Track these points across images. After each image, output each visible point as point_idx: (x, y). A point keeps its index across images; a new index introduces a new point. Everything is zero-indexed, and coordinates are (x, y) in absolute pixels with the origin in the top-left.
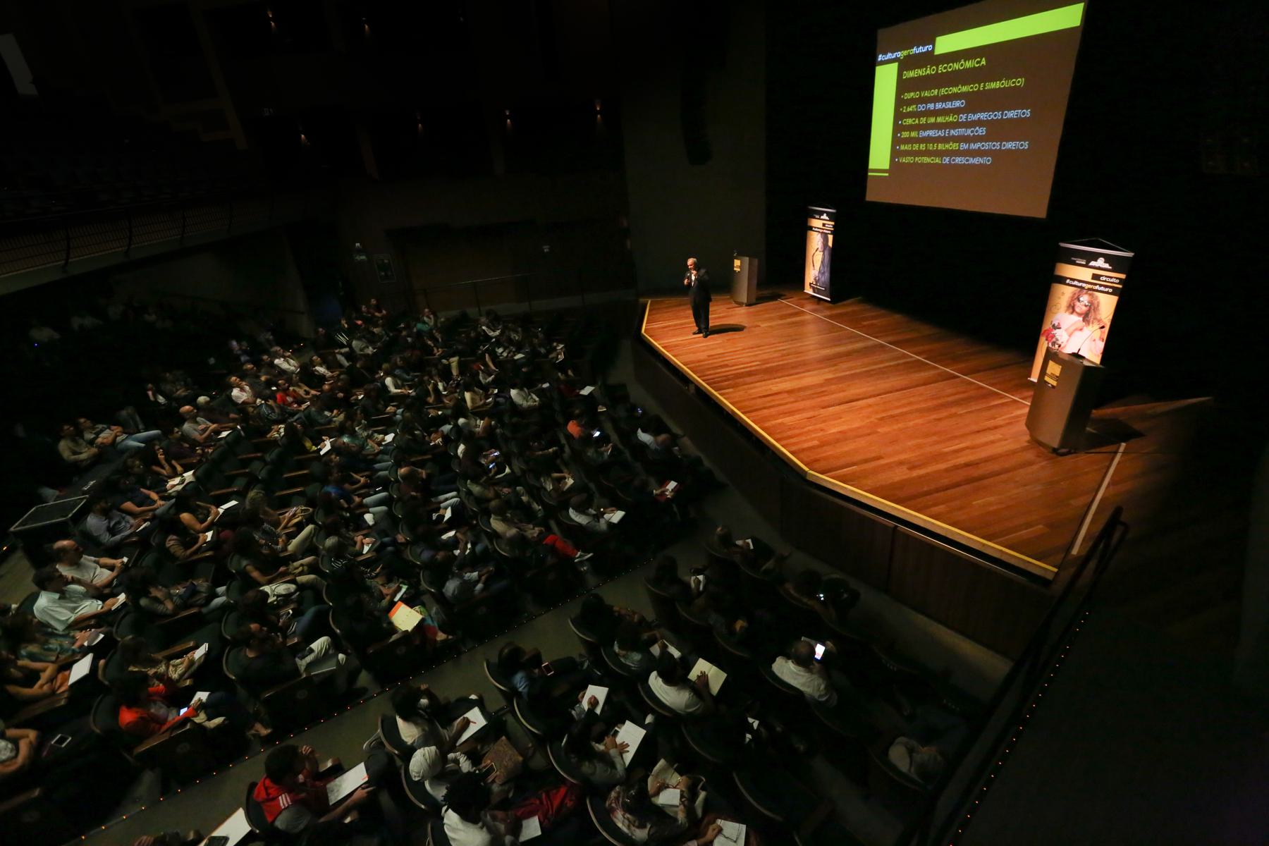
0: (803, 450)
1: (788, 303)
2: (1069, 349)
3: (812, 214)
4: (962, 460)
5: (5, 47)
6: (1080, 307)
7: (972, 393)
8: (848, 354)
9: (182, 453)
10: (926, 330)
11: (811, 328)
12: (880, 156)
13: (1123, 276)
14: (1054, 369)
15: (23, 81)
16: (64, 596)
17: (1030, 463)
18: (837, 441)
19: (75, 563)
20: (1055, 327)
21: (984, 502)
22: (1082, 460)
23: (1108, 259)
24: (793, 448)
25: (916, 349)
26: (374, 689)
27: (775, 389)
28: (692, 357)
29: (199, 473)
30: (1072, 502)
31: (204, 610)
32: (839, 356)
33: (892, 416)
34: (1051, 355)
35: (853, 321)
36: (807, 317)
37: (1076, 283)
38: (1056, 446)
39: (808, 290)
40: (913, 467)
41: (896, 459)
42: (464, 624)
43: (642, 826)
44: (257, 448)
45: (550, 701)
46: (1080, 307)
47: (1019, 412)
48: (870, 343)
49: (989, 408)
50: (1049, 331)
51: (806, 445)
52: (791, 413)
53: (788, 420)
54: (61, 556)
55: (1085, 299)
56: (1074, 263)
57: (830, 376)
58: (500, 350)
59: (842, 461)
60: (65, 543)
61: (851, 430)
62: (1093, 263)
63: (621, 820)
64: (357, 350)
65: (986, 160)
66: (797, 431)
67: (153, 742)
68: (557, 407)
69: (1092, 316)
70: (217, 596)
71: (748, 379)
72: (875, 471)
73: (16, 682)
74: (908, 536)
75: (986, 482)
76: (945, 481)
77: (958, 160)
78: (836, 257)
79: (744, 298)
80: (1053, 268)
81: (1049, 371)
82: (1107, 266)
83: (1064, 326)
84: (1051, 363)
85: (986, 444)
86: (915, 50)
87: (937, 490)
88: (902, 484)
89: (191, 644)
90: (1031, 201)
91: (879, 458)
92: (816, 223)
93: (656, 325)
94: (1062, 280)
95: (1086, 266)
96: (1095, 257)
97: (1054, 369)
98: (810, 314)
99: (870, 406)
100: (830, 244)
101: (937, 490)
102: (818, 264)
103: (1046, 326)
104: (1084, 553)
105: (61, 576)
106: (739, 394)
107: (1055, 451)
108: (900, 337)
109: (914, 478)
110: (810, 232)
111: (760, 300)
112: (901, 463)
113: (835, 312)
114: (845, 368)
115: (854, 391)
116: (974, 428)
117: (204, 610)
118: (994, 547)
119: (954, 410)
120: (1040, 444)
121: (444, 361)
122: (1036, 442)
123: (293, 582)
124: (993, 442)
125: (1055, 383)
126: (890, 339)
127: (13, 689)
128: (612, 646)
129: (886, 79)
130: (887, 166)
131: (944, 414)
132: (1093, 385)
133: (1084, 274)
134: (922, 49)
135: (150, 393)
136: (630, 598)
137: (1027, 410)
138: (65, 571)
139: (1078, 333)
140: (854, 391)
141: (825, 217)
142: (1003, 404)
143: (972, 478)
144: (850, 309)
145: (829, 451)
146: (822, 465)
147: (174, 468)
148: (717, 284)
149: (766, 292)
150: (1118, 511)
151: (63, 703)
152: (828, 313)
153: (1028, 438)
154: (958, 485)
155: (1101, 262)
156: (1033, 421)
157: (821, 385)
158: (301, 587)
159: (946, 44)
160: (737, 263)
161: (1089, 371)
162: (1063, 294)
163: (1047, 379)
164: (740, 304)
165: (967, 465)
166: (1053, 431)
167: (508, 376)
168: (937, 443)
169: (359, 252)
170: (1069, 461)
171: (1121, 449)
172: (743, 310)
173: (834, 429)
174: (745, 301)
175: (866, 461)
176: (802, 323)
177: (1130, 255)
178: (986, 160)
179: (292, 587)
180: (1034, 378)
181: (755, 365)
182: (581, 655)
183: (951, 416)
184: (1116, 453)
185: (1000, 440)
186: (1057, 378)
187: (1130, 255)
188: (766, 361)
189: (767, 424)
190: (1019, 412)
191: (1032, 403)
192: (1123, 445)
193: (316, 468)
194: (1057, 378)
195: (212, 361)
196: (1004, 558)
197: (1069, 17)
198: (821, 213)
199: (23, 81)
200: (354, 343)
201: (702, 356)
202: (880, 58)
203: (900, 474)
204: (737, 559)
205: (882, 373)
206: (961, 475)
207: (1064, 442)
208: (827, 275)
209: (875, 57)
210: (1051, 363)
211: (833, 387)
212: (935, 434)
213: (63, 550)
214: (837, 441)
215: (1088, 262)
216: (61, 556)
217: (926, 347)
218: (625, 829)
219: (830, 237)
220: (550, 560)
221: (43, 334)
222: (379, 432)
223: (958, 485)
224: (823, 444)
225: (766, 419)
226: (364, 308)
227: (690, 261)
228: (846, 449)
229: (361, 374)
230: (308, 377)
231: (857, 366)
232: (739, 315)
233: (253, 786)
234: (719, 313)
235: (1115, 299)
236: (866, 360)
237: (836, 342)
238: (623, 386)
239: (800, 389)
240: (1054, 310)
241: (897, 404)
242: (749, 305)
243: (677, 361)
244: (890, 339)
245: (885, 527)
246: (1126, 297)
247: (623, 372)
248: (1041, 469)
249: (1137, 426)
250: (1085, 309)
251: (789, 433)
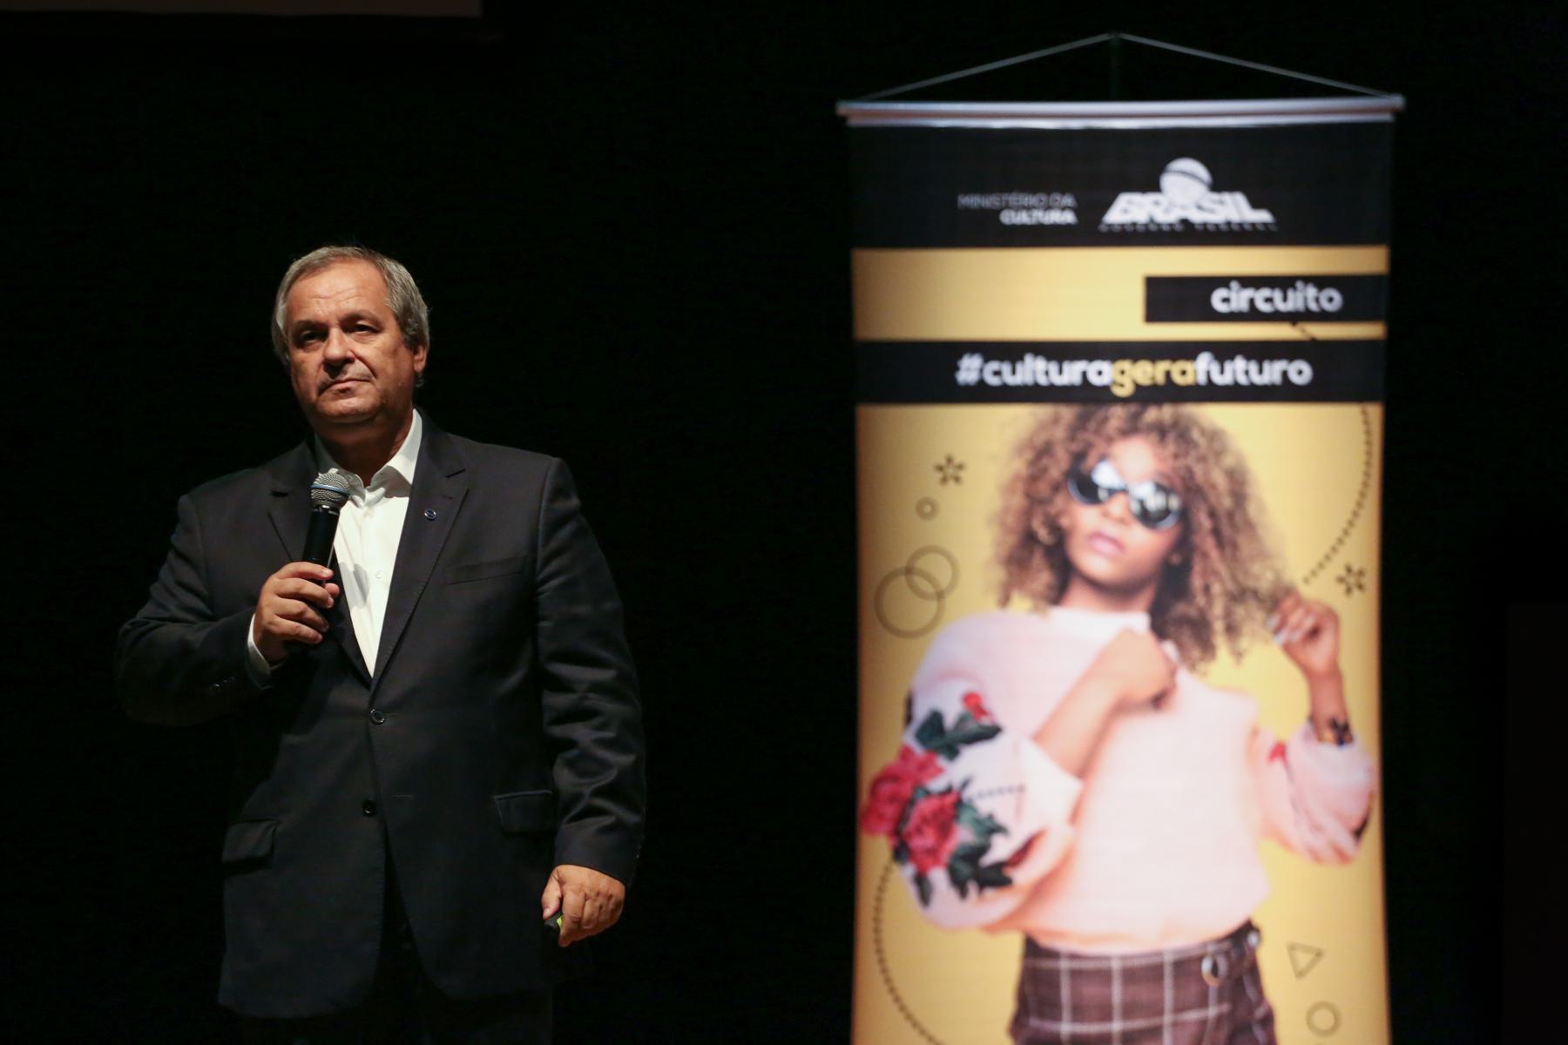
6: (1111, 539)
13: (1367, 260)
20: (943, 738)
23: (1228, 160)
37: (1033, 370)
46: (1111, 539)
50: (907, 775)
55: (1131, 467)
62: (1128, 209)
65: (1387, 117)
69: (1211, 586)
80: (837, 296)
82: (1235, 209)
94: (929, 373)
95: (1089, 232)
96: (1142, 161)
103: (885, 744)
133: (1079, 294)
139: (1140, 739)
155: (1185, 192)
162: (956, 473)
177: (863, 112)
187: (863, 112)
250: (1145, 544)
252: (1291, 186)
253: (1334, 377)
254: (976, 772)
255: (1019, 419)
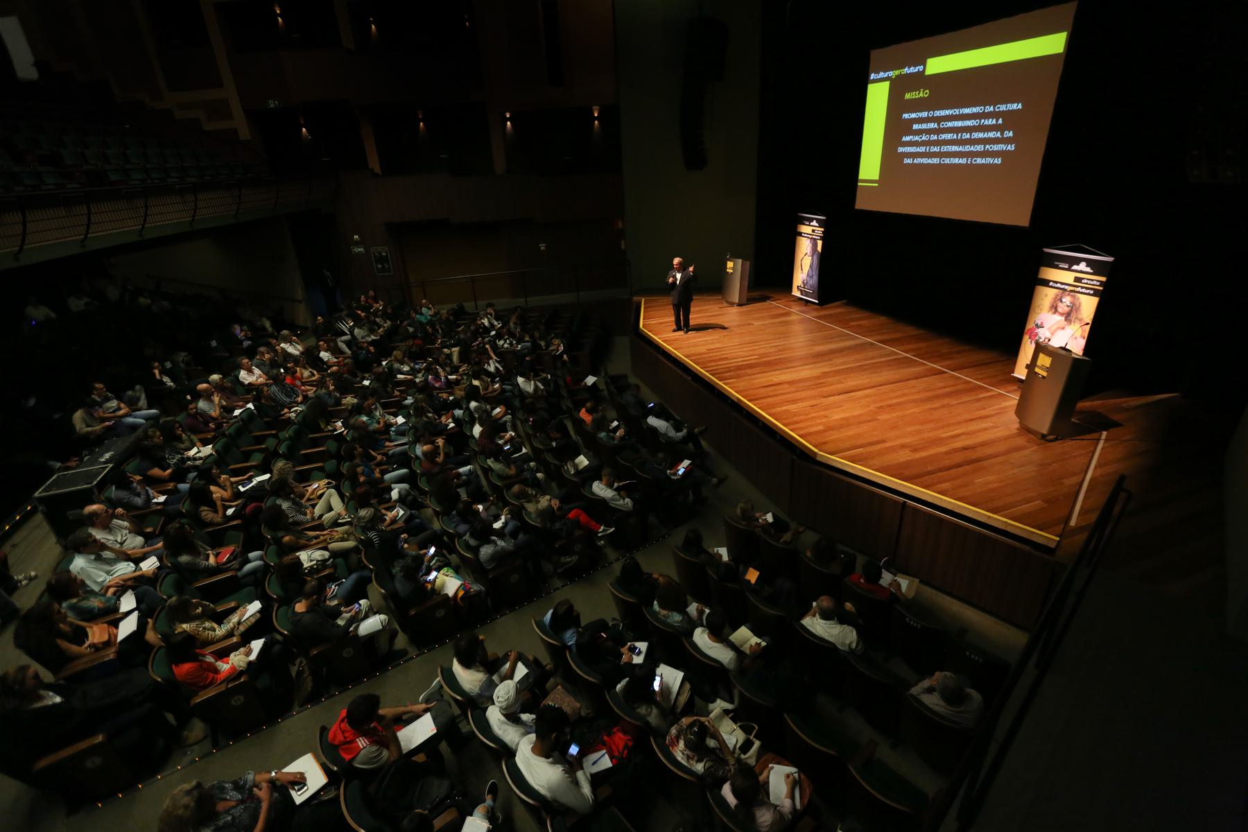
0: (811, 434)
1: (777, 305)
2: (1056, 342)
3: (802, 221)
4: (959, 444)
5: (10, 30)
6: (1063, 308)
7: (960, 387)
8: (840, 351)
9: (201, 428)
10: (911, 331)
11: (798, 328)
12: (870, 166)
13: (1104, 279)
14: (1044, 360)
15: (24, 64)
16: (99, 558)
17: (1024, 448)
18: (841, 427)
19: (107, 527)
20: (1038, 326)
21: (985, 481)
22: (1069, 446)
23: (1090, 263)
24: (801, 432)
25: (907, 347)
26: (413, 652)
27: (776, 380)
28: (693, 350)
29: (219, 445)
30: (1065, 481)
31: (239, 574)
32: (832, 352)
33: (890, 406)
34: (1040, 348)
35: (844, 323)
36: (793, 318)
38: (1045, 431)
39: (796, 293)
40: (915, 450)
41: (898, 442)
42: (502, 590)
43: (699, 761)
44: (269, 426)
45: (600, 649)
46: (1063, 308)
47: (1007, 404)
48: (857, 342)
49: (979, 400)
50: (1031, 331)
51: (813, 429)
52: (795, 401)
53: (792, 407)
54: (93, 520)
55: (1067, 300)
56: (1057, 267)
57: (826, 369)
58: (502, 342)
59: (848, 444)
60: (95, 507)
61: (853, 417)
62: (1075, 267)
63: (680, 752)
64: (359, 337)
65: (998, 161)
66: (802, 417)
67: (211, 693)
68: (564, 392)
69: (1073, 316)
70: (249, 561)
71: (749, 371)
72: (881, 453)
73: (63, 636)
74: (916, 510)
75: (984, 463)
76: (947, 462)
77: (979, 161)
78: (825, 262)
79: (736, 298)
80: (1037, 271)
81: (1039, 363)
82: (1088, 270)
83: (1047, 325)
84: (1041, 355)
85: (979, 431)
86: (906, 70)
87: (940, 470)
88: (908, 464)
89: (233, 604)
90: (1014, 210)
91: (884, 441)
92: (805, 229)
93: (652, 322)
94: (1046, 283)
95: (1069, 269)
96: (1078, 261)
97: (1044, 360)
98: (796, 312)
99: (867, 396)
100: (819, 249)
101: (940, 470)
102: (806, 268)
104: (1093, 517)
105: (95, 541)
106: (742, 384)
107: (1043, 436)
108: (886, 337)
109: (917, 460)
110: (799, 238)
111: (751, 301)
112: (903, 446)
113: (822, 313)
114: (839, 363)
115: (851, 382)
116: (967, 416)
117: (239, 574)
118: (998, 520)
119: (946, 401)
120: (1029, 431)
121: (446, 350)
122: (1025, 430)
123: (325, 549)
124: (985, 429)
125: (1045, 374)
126: (879, 338)
127: (64, 644)
128: (652, 605)
129: (877, 97)
130: (877, 178)
131: (937, 404)
132: (1086, 376)
134: (913, 70)
135: (157, 372)
136: (660, 565)
137: (1016, 402)
138: (99, 535)
139: (1060, 333)
140: (851, 382)
141: (814, 223)
142: (991, 397)
143: (970, 461)
144: (838, 311)
145: (835, 435)
146: (831, 447)
147: (191, 441)
148: (709, 284)
149: (755, 294)
150: (1122, 478)
151: (112, 657)
152: (815, 314)
153: (1017, 426)
154: (959, 466)
155: (1083, 266)
156: (1021, 410)
157: (819, 377)
158: (334, 554)
159: (937, 65)
160: (730, 264)
161: (1076, 361)
162: (1045, 296)
163: (1037, 370)
164: (732, 304)
165: (965, 449)
166: (1043, 420)
167: (513, 365)
168: (934, 429)
169: (357, 244)
170: (1058, 447)
171: (1103, 437)
172: (735, 309)
173: (837, 416)
174: (737, 300)
175: (870, 444)
176: (787, 323)
177: (1110, 259)
178: (998, 161)
179: (327, 554)
180: (1021, 373)
181: (753, 359)
182: (614, 619)
183: (943, 406)
184: (1099, 440)
185: (993, 427)
186: (1048, 370)
187: (1110, 259)
188: (765, 355)
189: (773, 411)
190: (1007, 404)
191: (1021, 397)
192: (1105, 433)
193: (332, 446)
194: (1048, 370)
195: (214, 343)
196: (1009, 529)
197: (1053, 44)
198: (811, 220)
199: (24, 64)
200: (356, 330)
201: (702, 349)
202: (873, 76)
203: (904, 456)
204: (758, 530)
205: (875, 368)
206: (959, 458)
207: (1050, 433)
208: (815, 278)
209: (868, 76)
210: (1041, 355)
211: (830, 379)
212: (931, 421)
213: (94, 514)
214: (841, 427)
215: (1071, 266)
216: (93, 520)
217: (912, 346)
218: (684, 763)
219: (820, 243)
220: (578, 533)
221: (39, 313)
222: (390, 414)
223: (959, 466)
224: (829, 429)
225: (774, 405)
226: (363, 298)
227: (676, 261)
228: (850, 433)
229: (362, 362)
230: (311, 358)
231: (850, 361)
232: (731, 315)
233: (324, 730)
234: (700, 312)
235: (1095, 300)
236: (858, 356)
237: (828, 339)
238: (625, 377)
239: (799, 381)
240: (1037, 310)
241: (892, 395)
242: (740, 305)
243: (678, 354)
244: (879, 338)
245: (897, 502)
246: (1106, 298)
247: (620, 363)
248: (1032, 453)
249: (1115, 417)
250: (1067, 309)
251: (796, 419)
252: (1097, 268)
253: (1096, 293)
254: (207, 785)
255: (1056, 291)
